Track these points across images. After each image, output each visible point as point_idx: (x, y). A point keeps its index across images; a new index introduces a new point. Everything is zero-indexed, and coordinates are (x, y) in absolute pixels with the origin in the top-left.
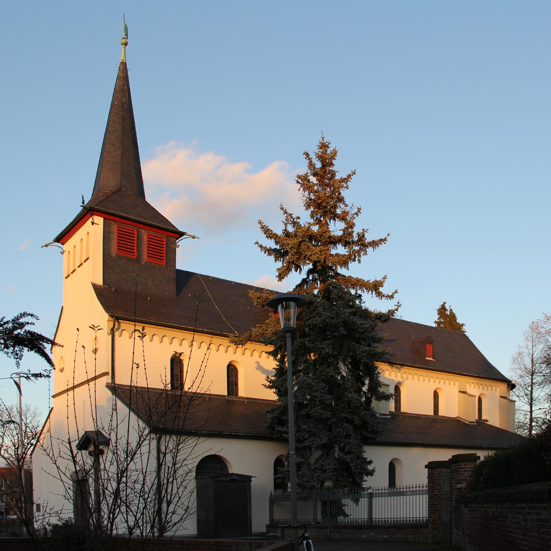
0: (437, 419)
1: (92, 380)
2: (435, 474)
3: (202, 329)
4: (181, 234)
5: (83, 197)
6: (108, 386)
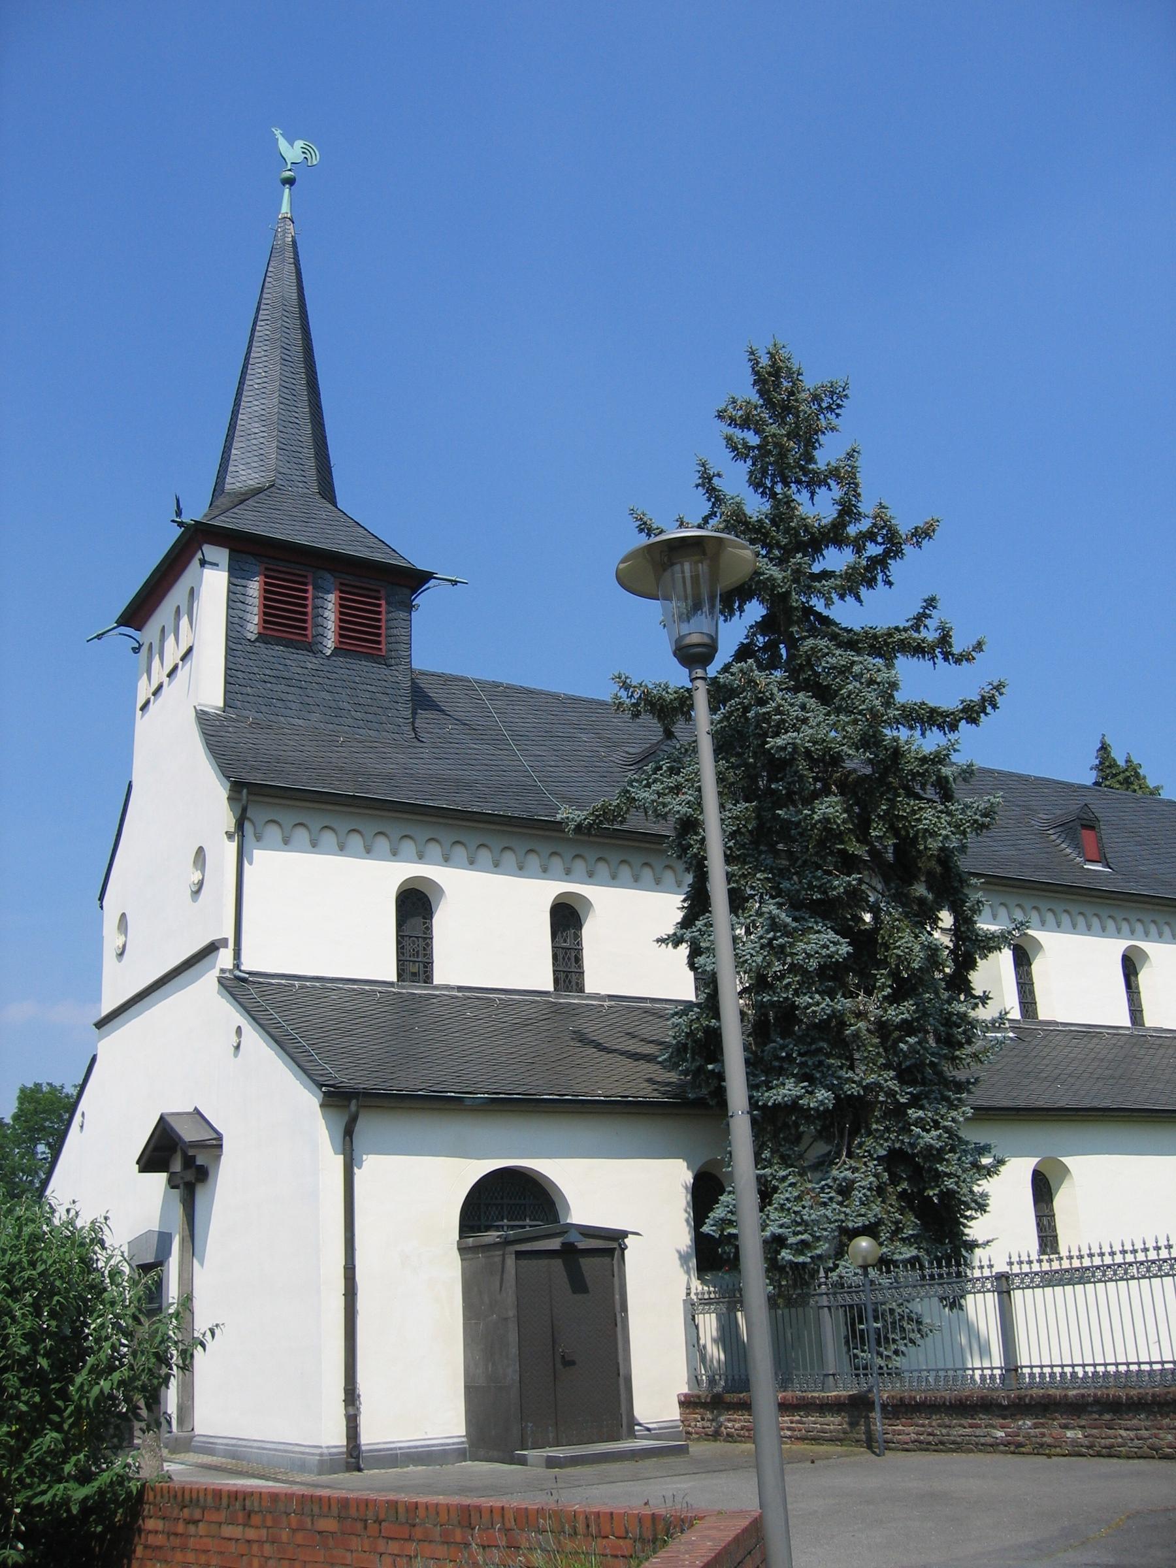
0: (1145, 1036)
4: (427, 577)
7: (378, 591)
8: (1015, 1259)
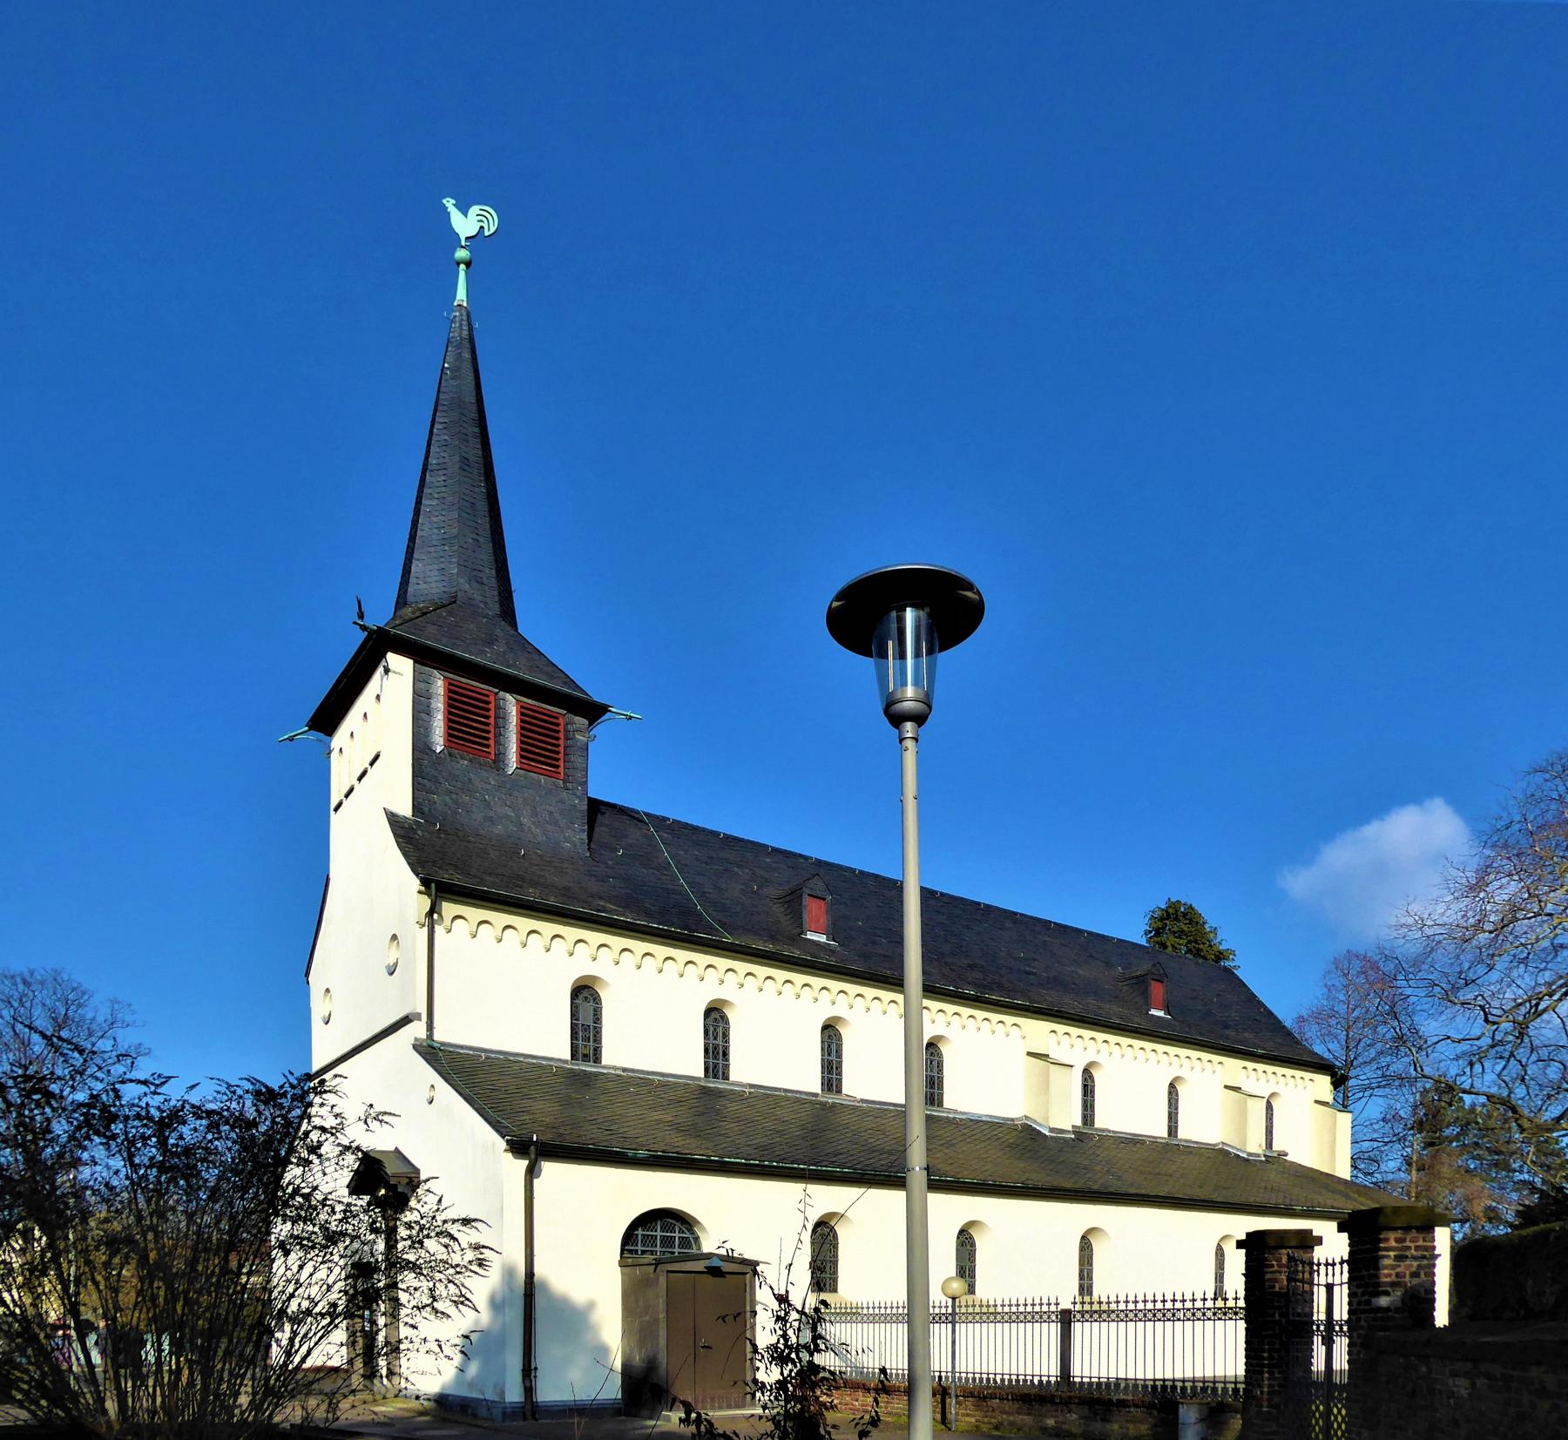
2: (1273, 1266)
3: (646, 924)
6: (417, 1047)
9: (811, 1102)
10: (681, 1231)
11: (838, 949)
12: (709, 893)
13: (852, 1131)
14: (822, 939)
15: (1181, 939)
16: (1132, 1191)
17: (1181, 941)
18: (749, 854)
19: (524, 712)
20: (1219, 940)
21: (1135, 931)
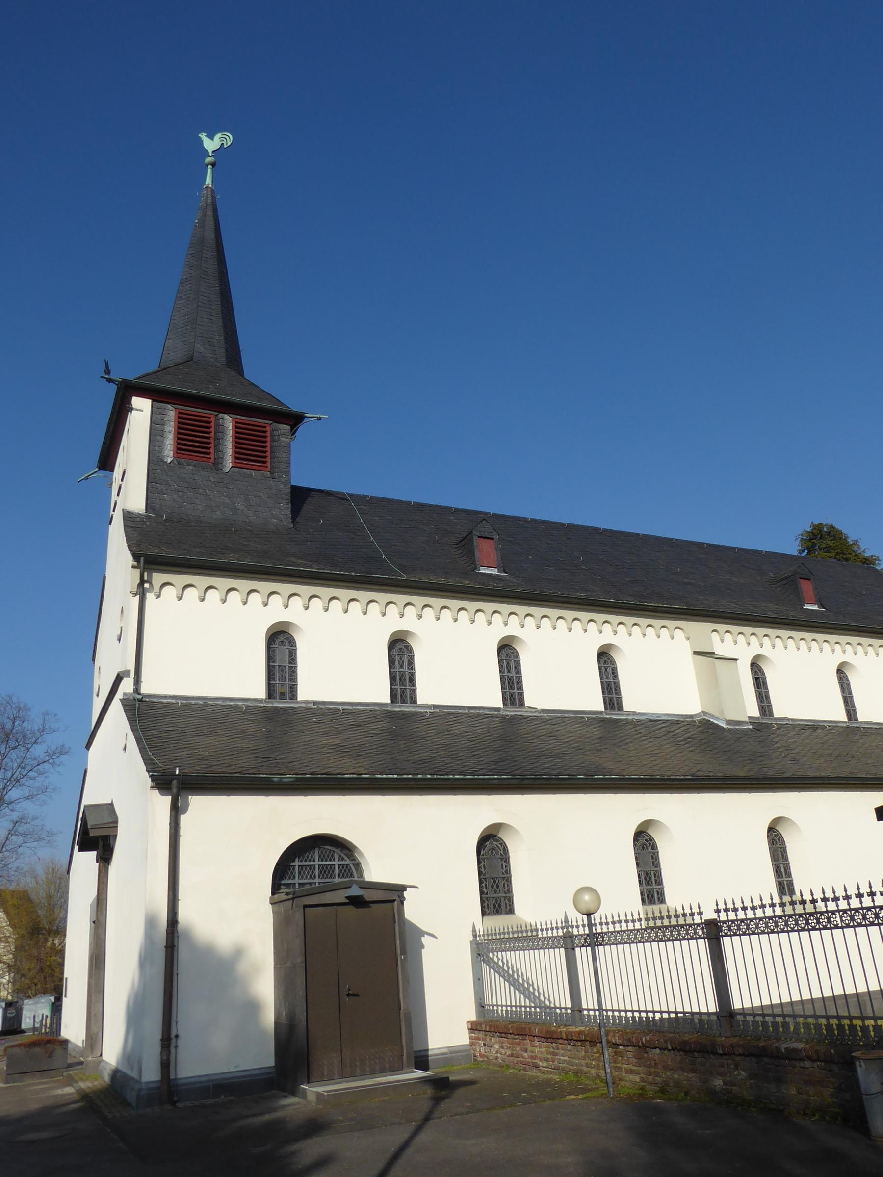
0: (859, 727)
1: (112, 695)
3: (329, 571)
5: (107, 364)
7: (265, 427)
8: (722, 906)
9: (492, 716)
10: (341, 858)
11: (509, 578)
12: (396, 545)
13: (524, 738)
14: (495, 571)
15: (831, 553)
16: (811, 774)
17: (831, 555)
18: (435, 515)
19: (238, 427)
20: (862, 550)
21: (792, 548)
